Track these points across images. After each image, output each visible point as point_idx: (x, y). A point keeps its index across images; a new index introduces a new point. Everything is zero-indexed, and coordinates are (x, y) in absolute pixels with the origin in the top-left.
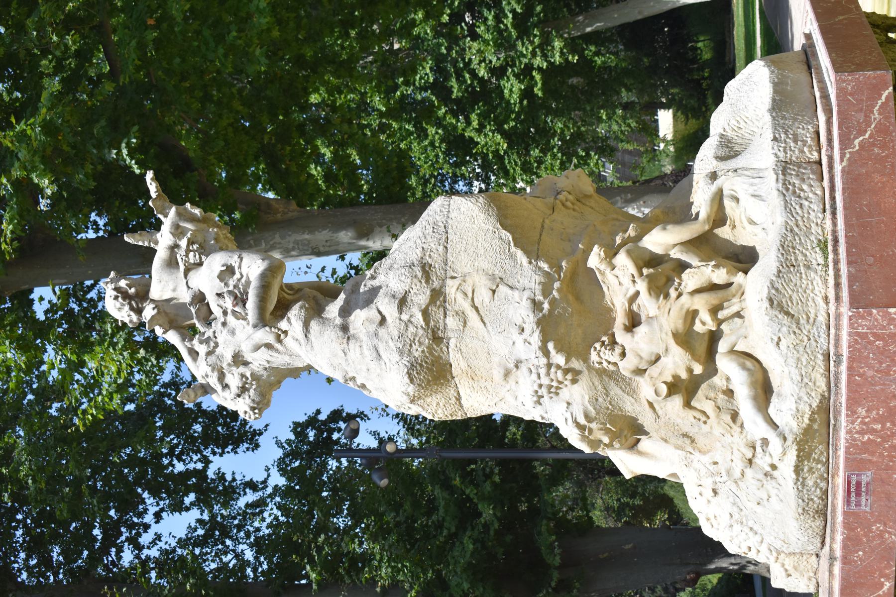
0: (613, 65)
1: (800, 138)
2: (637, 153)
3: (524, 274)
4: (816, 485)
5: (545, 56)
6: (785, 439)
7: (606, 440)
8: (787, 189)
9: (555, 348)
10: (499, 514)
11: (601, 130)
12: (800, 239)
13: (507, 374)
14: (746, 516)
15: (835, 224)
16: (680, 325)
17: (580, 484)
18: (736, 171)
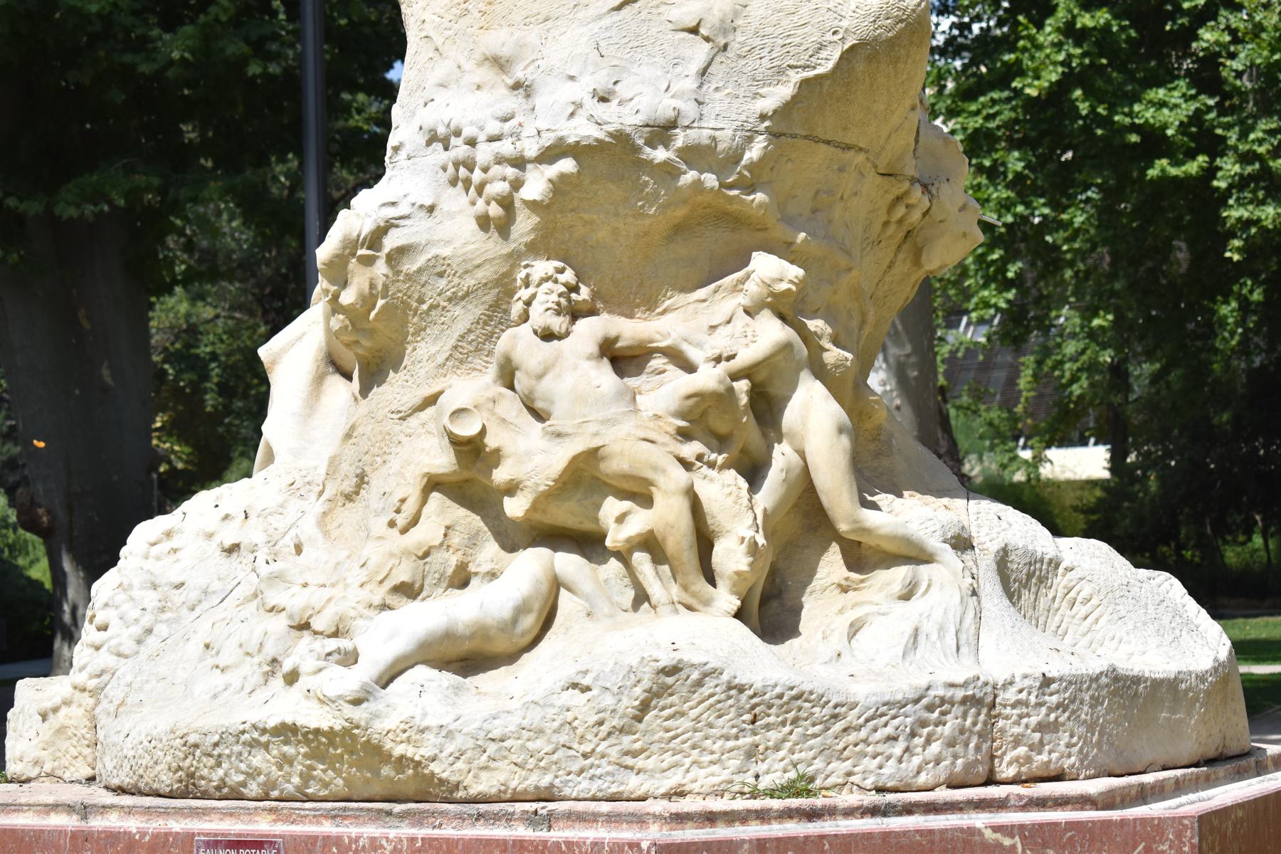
0: (1219, 344)
1: (1047, 737)
2: (1009, 401)
3: (736, 104)
4: (253, 774)
5: (1241, 183)
6: (357, 702)
7: (347, 297)
8: (930, 708)
9: (563, 177)
10: (170, 74)
11: (1066, 317)
12: (815, 736)
13: (499, 63)
14: (177, 620)
15: (849, 813)
16: (615, 465)
17: (247, 268)
18: (974, 593)
